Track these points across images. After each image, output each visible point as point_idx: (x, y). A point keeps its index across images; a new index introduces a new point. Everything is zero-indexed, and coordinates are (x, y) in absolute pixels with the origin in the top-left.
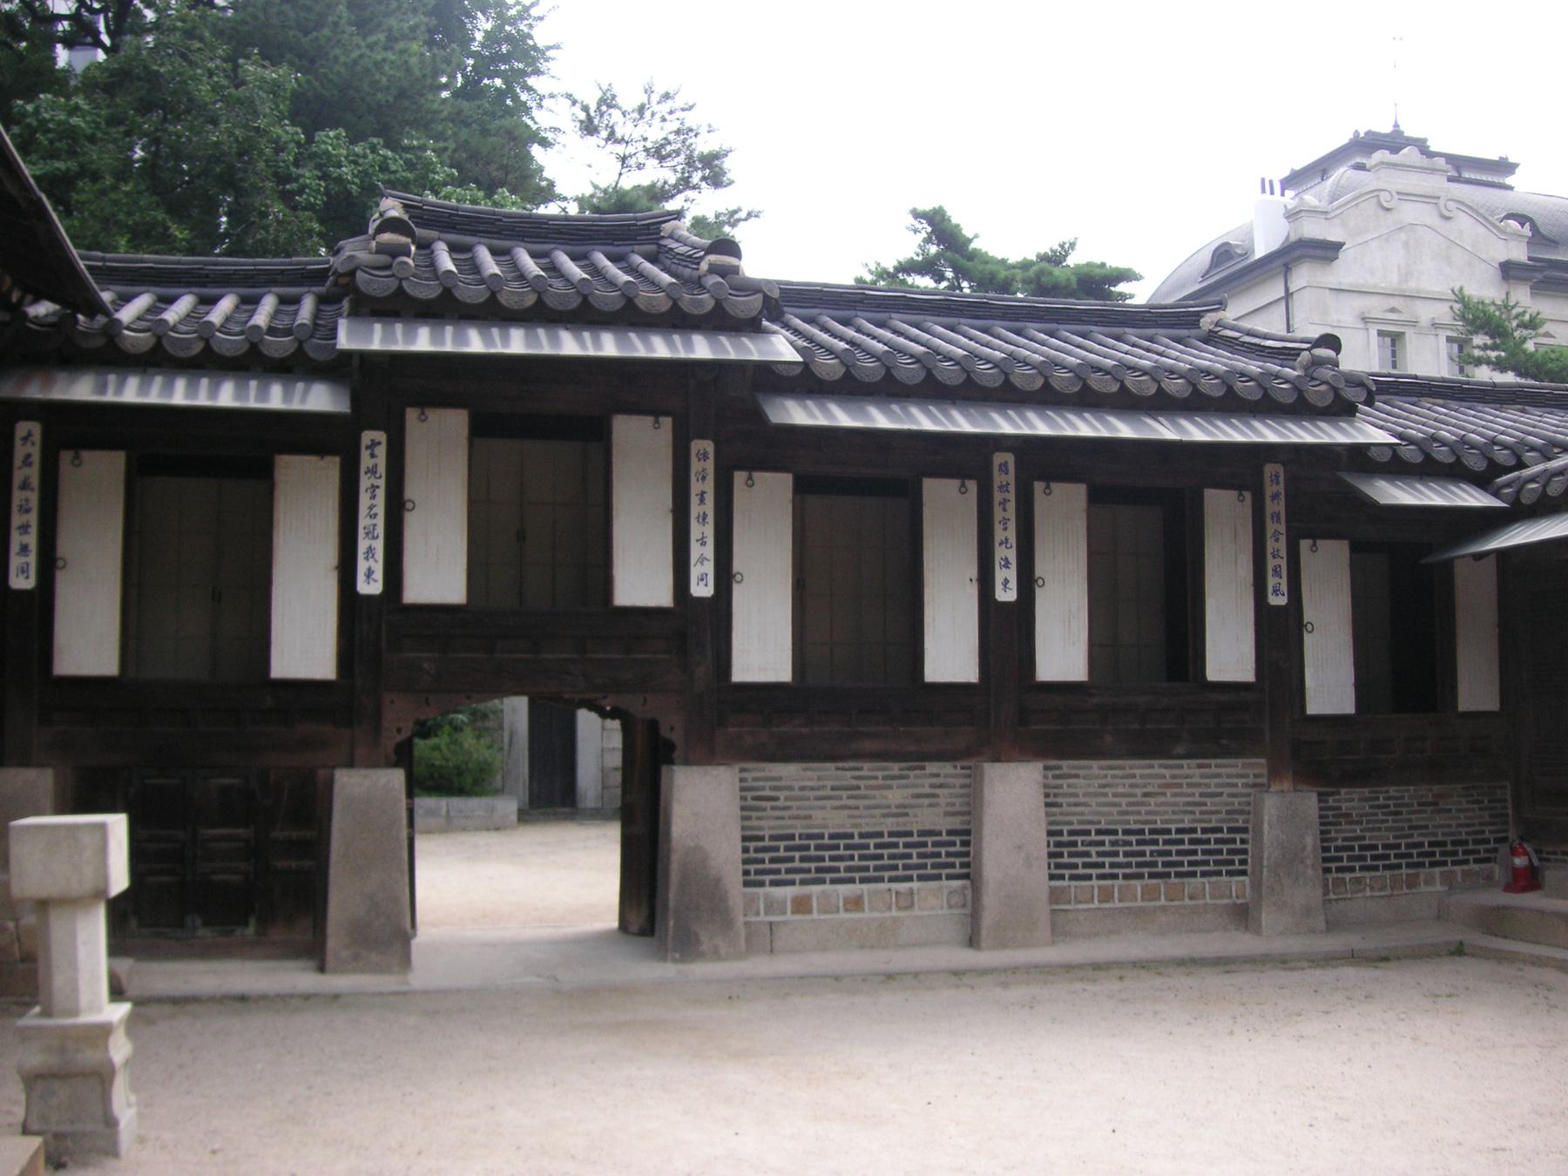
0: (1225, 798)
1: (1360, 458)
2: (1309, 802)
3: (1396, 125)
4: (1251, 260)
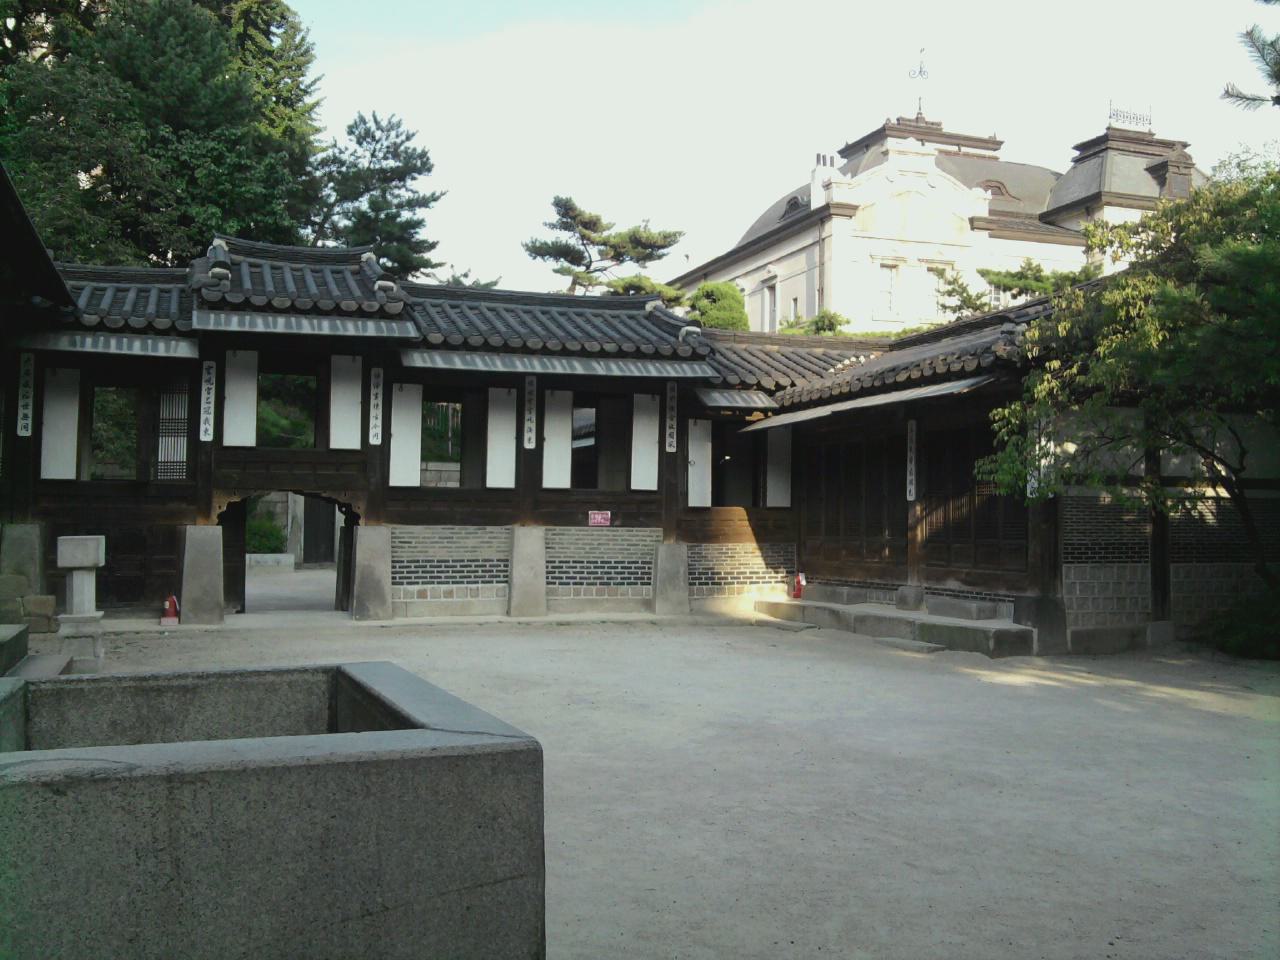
1: (707, 383)
2: (683, 549)
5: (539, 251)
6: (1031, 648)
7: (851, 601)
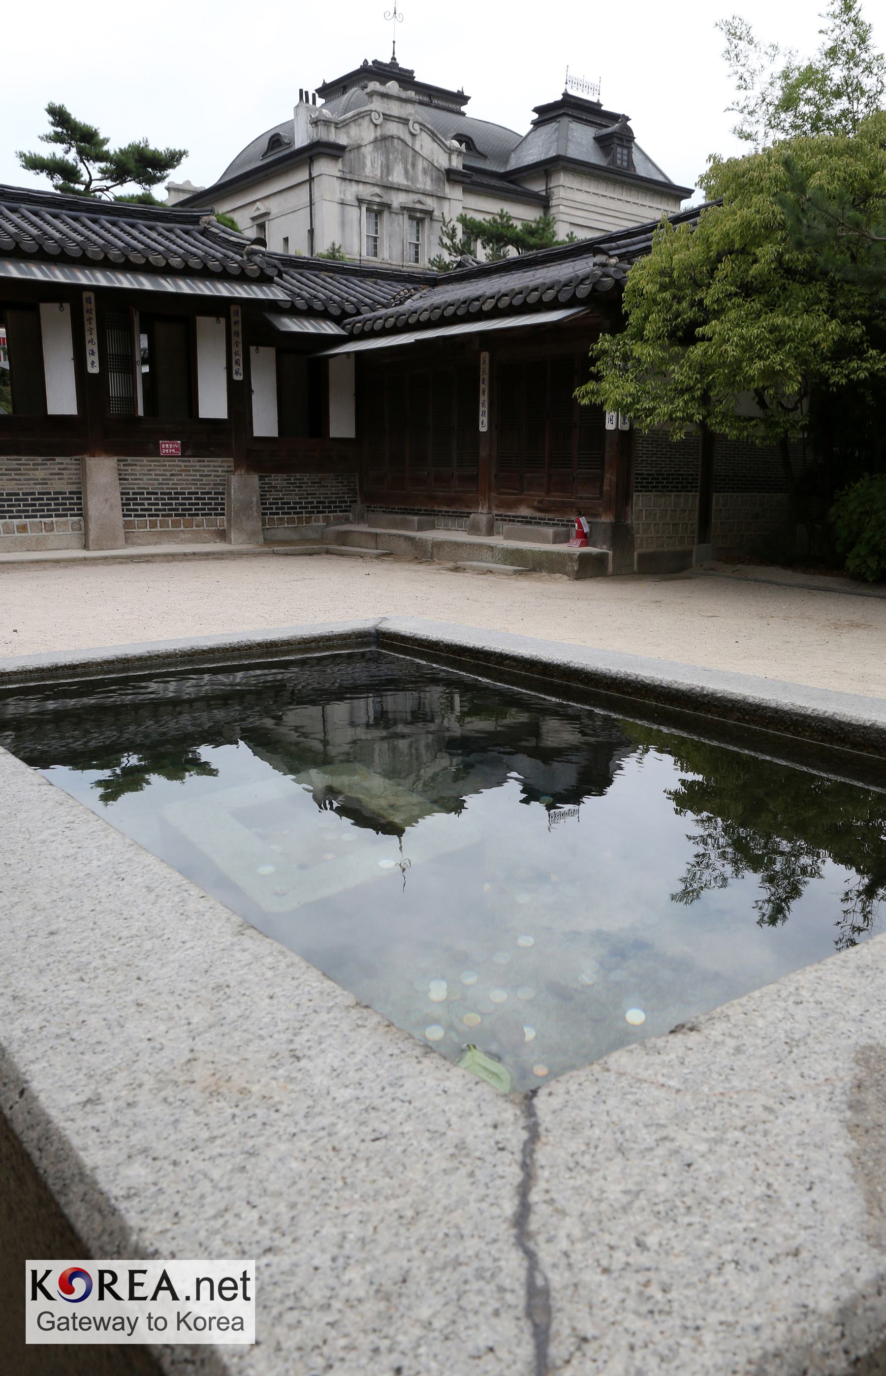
0: (212, 478)
1: (274, 306)
2: (254, 479)
3: (394, 59)
4: (292, 149)
5: (34, 164)
6: (606, 568)
7: (420, 529)
